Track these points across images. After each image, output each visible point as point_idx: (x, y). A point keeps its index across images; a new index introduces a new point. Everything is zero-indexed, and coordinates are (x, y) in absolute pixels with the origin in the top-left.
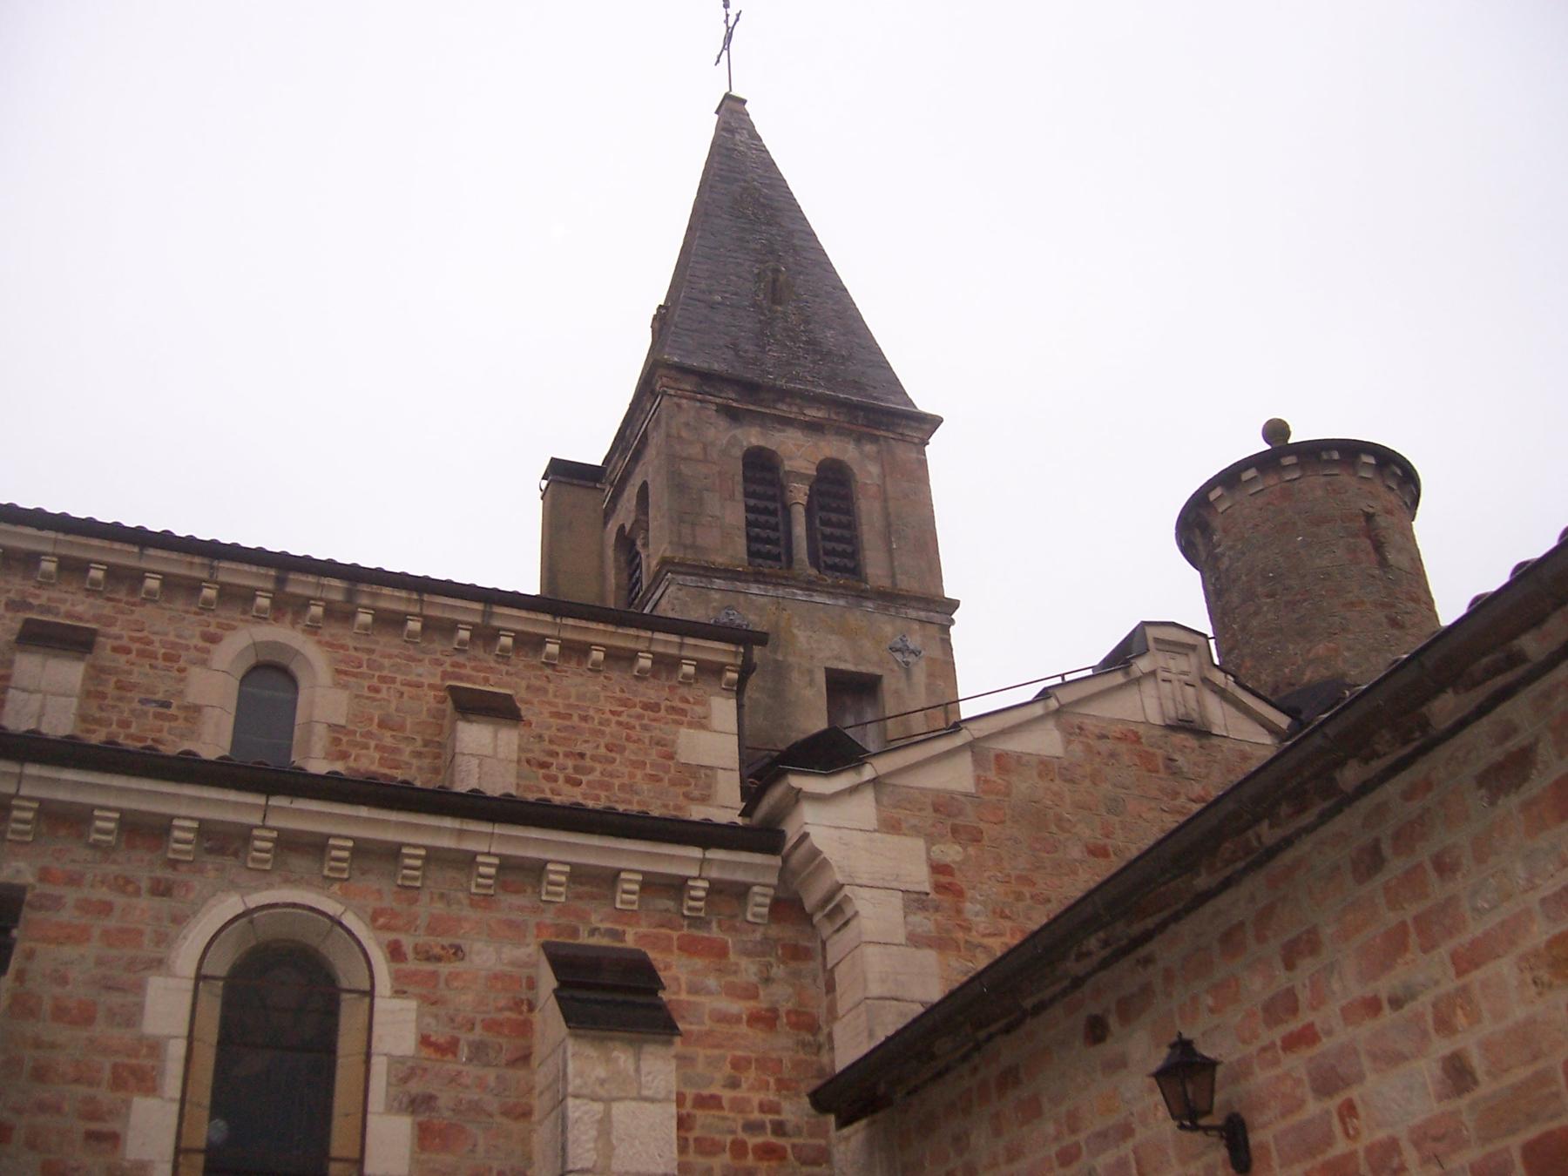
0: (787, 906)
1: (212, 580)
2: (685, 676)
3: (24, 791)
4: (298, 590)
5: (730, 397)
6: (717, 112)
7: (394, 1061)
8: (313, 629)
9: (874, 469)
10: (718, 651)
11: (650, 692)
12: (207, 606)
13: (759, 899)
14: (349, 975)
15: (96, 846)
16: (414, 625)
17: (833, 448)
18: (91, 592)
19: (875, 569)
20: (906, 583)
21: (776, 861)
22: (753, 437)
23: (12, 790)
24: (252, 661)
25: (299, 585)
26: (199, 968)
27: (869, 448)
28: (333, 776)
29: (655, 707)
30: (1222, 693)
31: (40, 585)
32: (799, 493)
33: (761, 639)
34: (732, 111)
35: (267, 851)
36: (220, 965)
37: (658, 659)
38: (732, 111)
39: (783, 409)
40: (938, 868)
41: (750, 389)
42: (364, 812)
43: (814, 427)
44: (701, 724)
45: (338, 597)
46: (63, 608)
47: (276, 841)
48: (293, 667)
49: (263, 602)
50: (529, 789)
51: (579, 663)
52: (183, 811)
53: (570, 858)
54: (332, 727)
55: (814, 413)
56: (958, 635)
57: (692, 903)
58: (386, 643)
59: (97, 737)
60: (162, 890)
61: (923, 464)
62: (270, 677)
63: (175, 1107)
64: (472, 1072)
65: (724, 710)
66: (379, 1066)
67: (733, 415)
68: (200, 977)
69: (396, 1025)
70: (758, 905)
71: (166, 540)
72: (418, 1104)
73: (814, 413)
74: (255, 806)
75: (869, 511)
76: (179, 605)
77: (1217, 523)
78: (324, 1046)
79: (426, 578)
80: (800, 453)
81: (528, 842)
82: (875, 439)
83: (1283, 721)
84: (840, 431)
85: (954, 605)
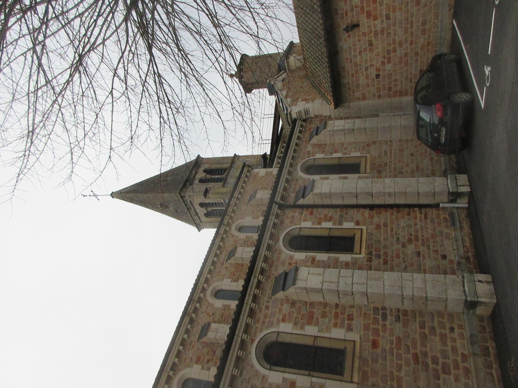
1: (222, 235)
2: (203, 296)
4: (197, 298)
6: (113, 198)
8: (233, 222)
9: (206, 165)
10: (246, 169)
12: (227, 237)
19: (225, 166)
21: (298, 121)
22: (197, 182)
26: (268, 369)
27: (202, 166)
30: (278, 77)
31: (219, 261)
32: (208, 176)
33: (245, 163)
34: (113, 195)
36: (268, 366)
37: (202, 292)
38: (113, 195)
40: (302, 101)
43: (196, 173)
44: (258, 173)
45: (228, 217)
46: (224, 257)
47: (261, 275)
48: (185, 378)
50: (216, 363)
52: (264, 253)
53: (232, 367)
54: (253, 219)
55: (194, 172)
56: (241, 154)
60: (297, 180)
62: (219, 294)
63: (299, 376)
65: (255, 171)
68: (270, 369)
69: (286, 327)
72: (331, 153)
73: (194, 172)
75: (214, 167)
77: (247, 81)
80: (201, 174)
81: (254, 281)
82: (200, 165)
83: (283, 71)
84: (198, 169)
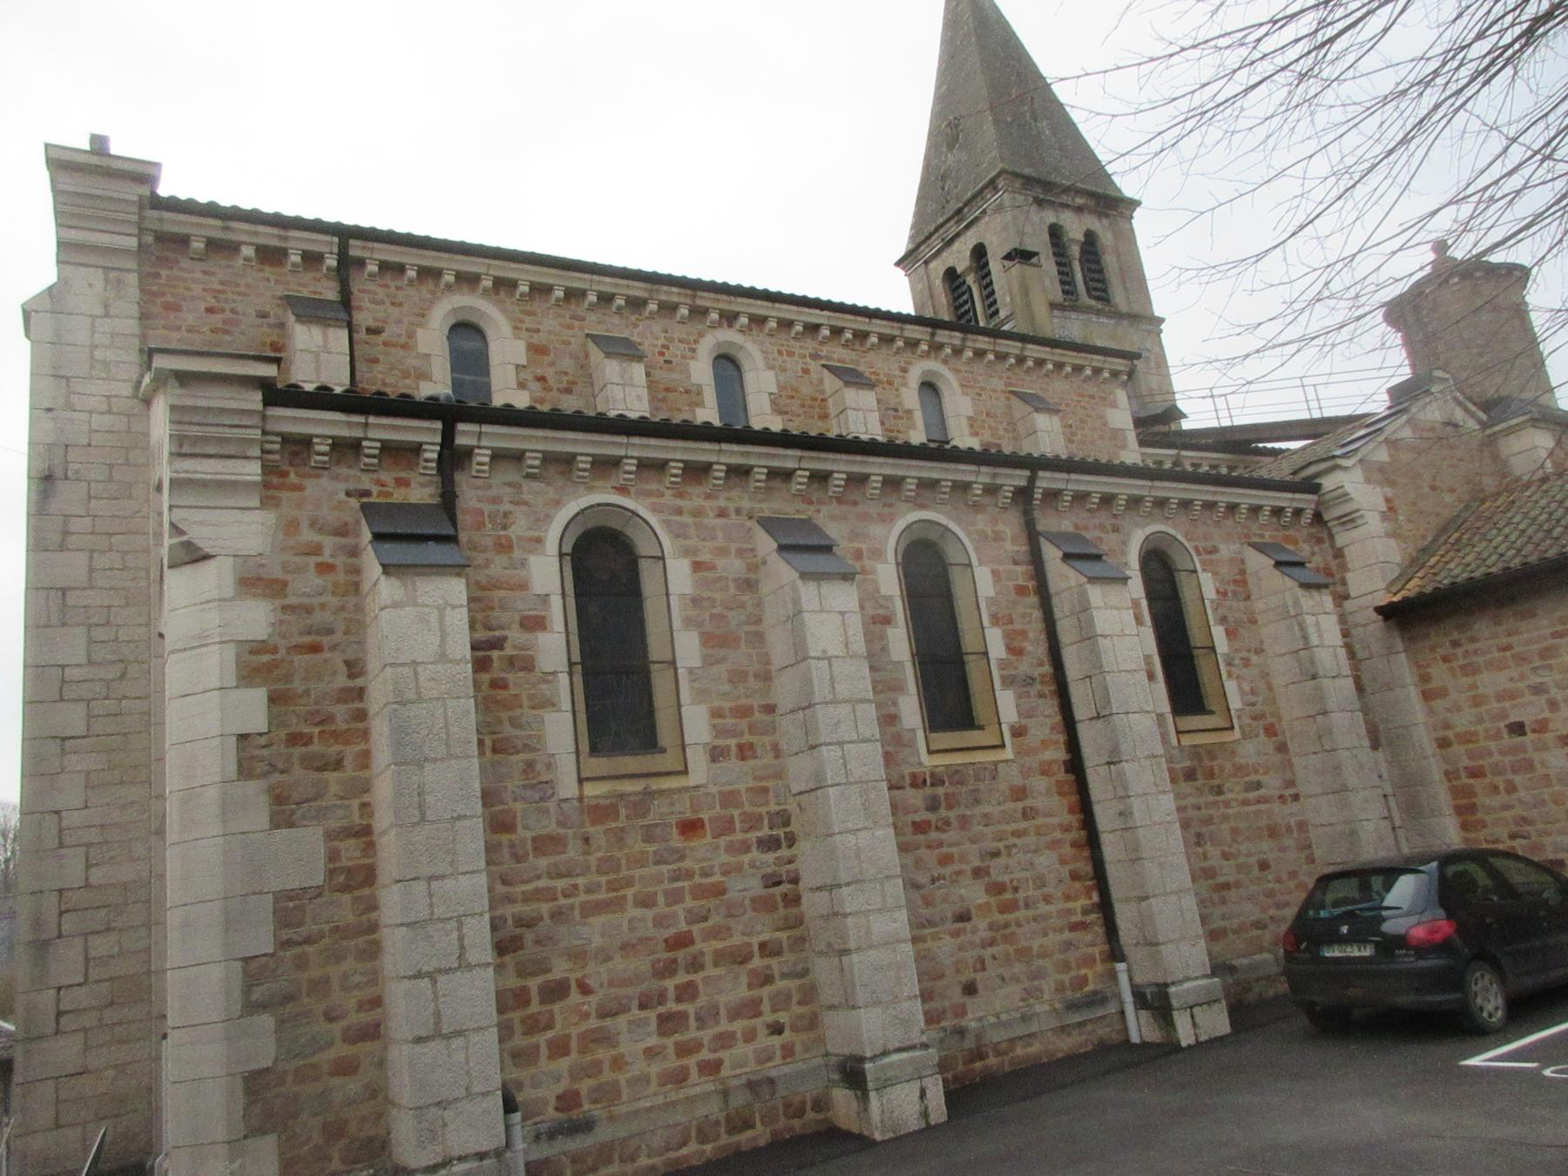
0: (1318, 517)
3: (483, 443)
5: (1038, 192)
7: (1212, 601)
8: (945, 362)
11: (1090, 389)
13: (675, 471)
14: (644, 547)
15: (1089, 510)
16: (684, 311)
17: (1091, 222)
18: (845, 346)
19: (1118, 296)
20: (1136, 309)
22: (1050, 217)
23: (474, 443)
24: (452, 321)
25: (705, 300)
27: (1105, 222)
28: (785, 432)
29: (1092, 397)
31: (822, 343)
35: (374, 456)
36: (568, 548)
37: (722, 314)
39: (1065, 199)
41: (1047, 186)
42: (1184, 486)
43: (1079, 210)
44: (1114, 405)
49: (924, 347)
51: (862, 345)
55: (1079, 201)
57: (367, 460)
58: (979, 368)
59: (545, 408)
60: (1116, 529)
61: (1132, 230)
64: (1234, 604)
65: (1121, 396)
66: (675, 602)
67: (1039, 202)
68: (561, 555)
70: (1307, 517)
71: (254, 217)
72: (1223, 620)
74: (358, 424)
75: (1110, 261)
76: (884, 350)
78: (634, 591)
79: (499, 249)
80: (1075, 227)
82: (1107, 216)
85: (1161, 320)
